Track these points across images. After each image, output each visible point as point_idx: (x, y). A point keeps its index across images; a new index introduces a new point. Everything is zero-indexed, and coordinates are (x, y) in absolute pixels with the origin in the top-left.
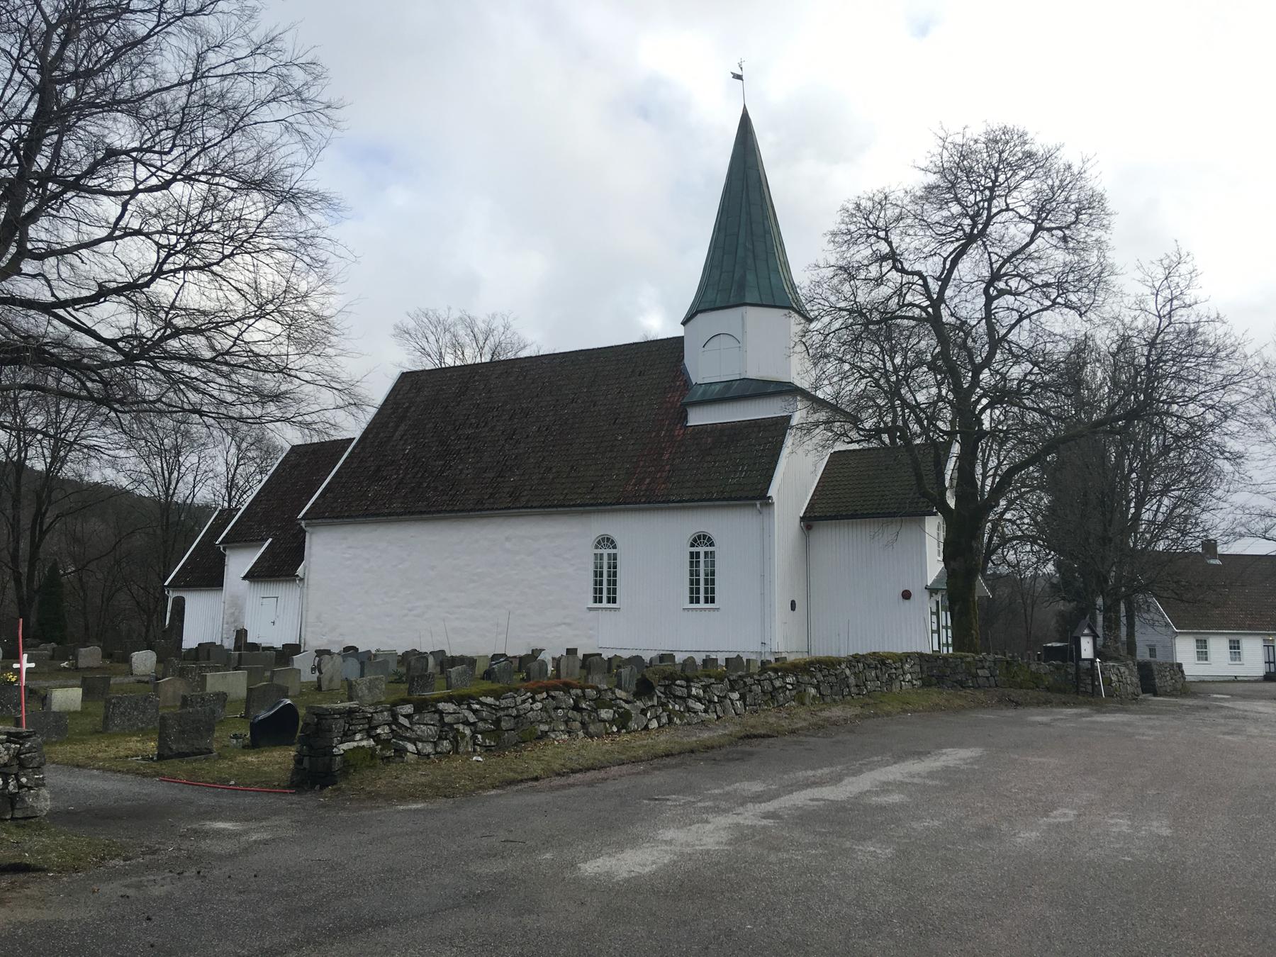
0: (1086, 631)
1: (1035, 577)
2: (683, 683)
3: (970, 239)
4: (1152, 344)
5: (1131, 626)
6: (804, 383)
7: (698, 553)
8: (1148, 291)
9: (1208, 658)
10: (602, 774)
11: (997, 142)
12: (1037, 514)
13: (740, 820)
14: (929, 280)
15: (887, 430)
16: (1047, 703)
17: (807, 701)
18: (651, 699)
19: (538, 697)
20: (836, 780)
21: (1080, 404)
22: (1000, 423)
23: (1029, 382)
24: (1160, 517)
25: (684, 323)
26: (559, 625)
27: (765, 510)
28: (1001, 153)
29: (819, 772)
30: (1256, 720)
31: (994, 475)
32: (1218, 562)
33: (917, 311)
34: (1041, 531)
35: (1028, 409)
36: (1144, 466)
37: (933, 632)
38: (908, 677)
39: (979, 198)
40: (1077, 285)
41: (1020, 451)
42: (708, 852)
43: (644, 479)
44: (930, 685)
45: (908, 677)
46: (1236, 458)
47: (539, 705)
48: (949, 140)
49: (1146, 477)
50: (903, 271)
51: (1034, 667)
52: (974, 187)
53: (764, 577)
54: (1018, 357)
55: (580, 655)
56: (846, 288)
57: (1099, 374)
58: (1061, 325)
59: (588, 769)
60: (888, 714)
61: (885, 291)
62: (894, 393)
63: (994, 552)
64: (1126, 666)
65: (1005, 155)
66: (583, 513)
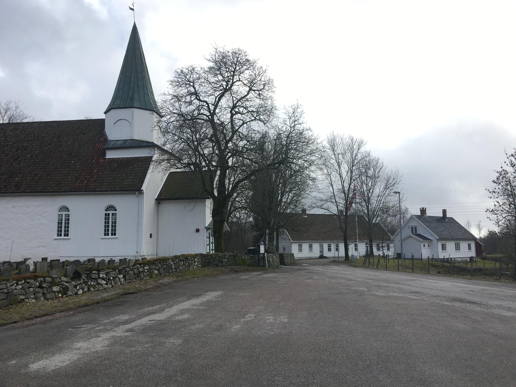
0: (262, 243)
1: (246, 223)
2: (96, 272)
3: (226, 90)
4: (288, 137)
5: (277, 240)
6: (159, 143)
7: (109, 214)
8: (287, 117)
9: (301, 251)
10: (51, 317)
11: (236, 54)
12: (247, 199)
13: (115, 334)
14: (210, 105)
15: (192, 164)
16: (248, 271)
17: (154, 276)
18: (80, 280)
19: (20, 283)
20: (162, 310)
21: (263, 158)
22: (235, 163)
23: (246, 148)
24: (289, 201)
25: (105, 113)
26: (39, 247)
27: (140, 196)
28: (238, 58)
29: (155, 307)
30: (317, 273)
31: (233, 184)
32: (306, 217)
33: (205, 117)
34: (248, 205)
35: (245, 158)
36: (284, 182)
37: (207, 245)
38: (196, 263)
39: (229, 75)
40: (264, 113)
41: (242, 175)
42: (97, 352)
43: (84, 181)
44: (205, 267)
45: (196, 263)
46: (313, 180)
47: (20, 287)
48: (218, 50)
49: (284, 186)
50: (200, 100)
51: (243, 257)
52: (227, 70)
53: (139, 224)
54: (242, 138)
55: (49, 260)
56: (177, 104)
57: (270, 147)
58: (257, 126)
59: (44, 316)
60: (187, 279)
61: (192, 107)
62: (196, 150)
63: (231, 213)
64: (275, 255)
65: (239, 59)
66: (53, 195)
